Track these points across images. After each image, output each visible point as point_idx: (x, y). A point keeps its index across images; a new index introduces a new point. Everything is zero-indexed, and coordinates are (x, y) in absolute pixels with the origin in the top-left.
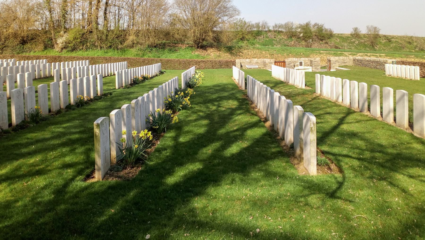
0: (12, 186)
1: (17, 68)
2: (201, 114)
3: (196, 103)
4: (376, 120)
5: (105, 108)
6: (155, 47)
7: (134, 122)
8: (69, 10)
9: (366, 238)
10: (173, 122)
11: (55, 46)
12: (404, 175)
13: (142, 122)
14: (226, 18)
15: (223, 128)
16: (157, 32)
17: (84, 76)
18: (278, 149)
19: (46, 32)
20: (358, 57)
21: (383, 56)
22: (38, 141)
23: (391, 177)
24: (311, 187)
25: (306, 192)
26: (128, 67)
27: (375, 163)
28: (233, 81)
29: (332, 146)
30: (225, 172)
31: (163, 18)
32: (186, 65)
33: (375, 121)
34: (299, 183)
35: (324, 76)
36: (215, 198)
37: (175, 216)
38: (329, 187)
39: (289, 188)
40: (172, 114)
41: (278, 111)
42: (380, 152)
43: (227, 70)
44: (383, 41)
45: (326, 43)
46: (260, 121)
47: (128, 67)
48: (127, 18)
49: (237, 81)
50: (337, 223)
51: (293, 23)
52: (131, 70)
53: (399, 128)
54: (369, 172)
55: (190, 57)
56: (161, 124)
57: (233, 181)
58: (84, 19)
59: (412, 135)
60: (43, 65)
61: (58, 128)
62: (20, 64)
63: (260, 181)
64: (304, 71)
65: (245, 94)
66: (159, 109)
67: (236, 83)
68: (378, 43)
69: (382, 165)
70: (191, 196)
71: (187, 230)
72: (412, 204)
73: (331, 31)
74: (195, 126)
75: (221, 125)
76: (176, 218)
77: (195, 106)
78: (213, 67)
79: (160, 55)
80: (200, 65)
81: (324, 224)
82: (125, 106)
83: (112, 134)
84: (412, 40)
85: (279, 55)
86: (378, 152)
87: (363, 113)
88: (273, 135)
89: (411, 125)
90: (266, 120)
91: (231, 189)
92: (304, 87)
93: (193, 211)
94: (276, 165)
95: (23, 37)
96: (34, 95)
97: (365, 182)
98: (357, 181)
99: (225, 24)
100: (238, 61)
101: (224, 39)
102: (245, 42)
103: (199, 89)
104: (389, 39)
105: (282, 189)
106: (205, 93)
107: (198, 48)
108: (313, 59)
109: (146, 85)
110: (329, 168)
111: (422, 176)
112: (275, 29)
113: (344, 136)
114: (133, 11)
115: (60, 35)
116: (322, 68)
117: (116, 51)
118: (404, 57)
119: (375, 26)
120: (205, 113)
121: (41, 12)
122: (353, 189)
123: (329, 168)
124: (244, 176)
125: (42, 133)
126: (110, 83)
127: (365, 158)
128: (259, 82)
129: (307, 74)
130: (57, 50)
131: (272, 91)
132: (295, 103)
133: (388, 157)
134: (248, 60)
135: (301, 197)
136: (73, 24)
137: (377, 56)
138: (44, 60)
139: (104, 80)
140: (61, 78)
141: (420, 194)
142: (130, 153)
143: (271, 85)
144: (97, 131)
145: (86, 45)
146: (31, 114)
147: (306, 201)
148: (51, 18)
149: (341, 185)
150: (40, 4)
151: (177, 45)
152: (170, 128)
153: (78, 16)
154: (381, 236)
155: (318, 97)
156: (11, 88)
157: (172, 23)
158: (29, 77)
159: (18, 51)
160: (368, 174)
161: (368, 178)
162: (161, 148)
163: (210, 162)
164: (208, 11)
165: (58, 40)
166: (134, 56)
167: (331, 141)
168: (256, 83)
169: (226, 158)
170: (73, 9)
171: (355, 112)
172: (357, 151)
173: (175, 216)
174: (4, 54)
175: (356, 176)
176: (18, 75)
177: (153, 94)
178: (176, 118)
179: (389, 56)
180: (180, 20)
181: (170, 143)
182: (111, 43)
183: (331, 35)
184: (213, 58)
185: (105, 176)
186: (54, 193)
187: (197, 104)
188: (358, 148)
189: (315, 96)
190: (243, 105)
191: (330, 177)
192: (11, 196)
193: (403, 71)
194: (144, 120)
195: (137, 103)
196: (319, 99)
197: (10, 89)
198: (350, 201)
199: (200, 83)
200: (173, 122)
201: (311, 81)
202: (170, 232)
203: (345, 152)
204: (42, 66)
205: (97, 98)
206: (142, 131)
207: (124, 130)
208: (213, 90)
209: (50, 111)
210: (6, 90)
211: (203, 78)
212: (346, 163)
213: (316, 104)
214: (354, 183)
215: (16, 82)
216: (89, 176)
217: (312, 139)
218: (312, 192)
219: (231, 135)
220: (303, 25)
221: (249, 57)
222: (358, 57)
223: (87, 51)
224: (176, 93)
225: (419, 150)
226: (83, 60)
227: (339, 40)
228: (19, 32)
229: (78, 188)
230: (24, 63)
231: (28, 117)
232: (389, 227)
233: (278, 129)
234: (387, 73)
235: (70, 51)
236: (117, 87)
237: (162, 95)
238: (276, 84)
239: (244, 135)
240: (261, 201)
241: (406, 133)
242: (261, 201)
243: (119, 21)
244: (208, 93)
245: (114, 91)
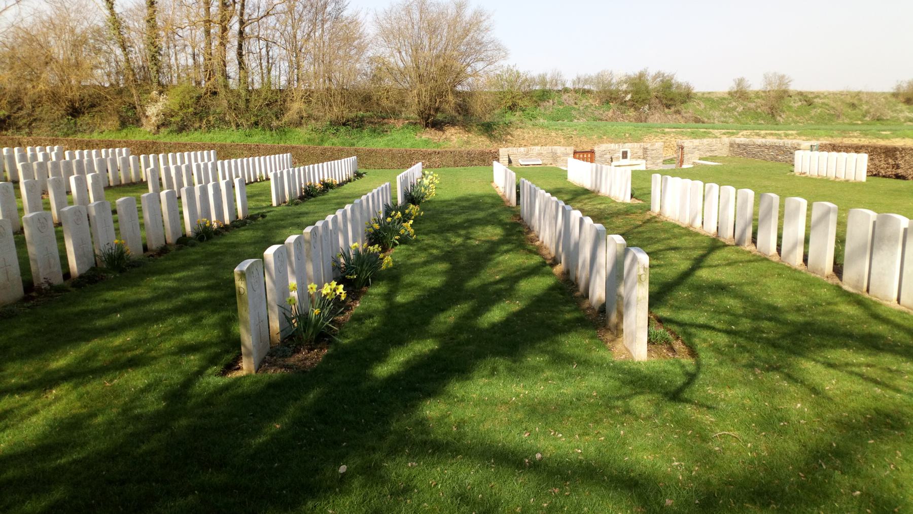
0: (82, 389)
1: (68, 165)
2: (435, 251)
4: (767, 260)
5: (254, 243)
6: (344, 124)
7: (310, 268)
8: (164, 44)
9: (736, 472)
10: (384, 267)
11: (144, 120)
12: (817, 361)
13: (326, 267)
14: (480, 66)
16: (348, 95)
17: (208, 182)
19: (120, 92)
20: (741, 138)
21: (792, 135)
22: (126, 306)
23: (789, 366)
24: (637, 382)
25: (627, 390)
26: (294, 165)
27: (760, 340)
29: (679, 308)
30: (480, 356)
31: (358, 66)
32: (405, 160)
33: (766, 262)
34: (613, 375)
35: (669, 177)
36: (462, 400)
37: (391, 433)
38: (669, 381)
40: (380, 252)
41: (577, 245)
42: (770, 319)
44: (796, 105)
45: (678, 112)
46: (544, 264)
47: (294, 165)
48: (285, 65)
50: (683, 446)
52: (299, 170)
53: (813, 275)
54: (747, 355)
55: (413, 144)
56: (361, 271)
57: (493, 372)
58: (196, 65)
60: (123, 159)
61: (164, 280)
62: (72, 156)
63: (543, 371)
65: (516, 213)
66: (356, 244)
67: (500, 194)
68: (785, 109)
69: (773, 344)
70: (419, 399)
71: (412, 456)
72: (829, 415)
74: (424, 274)
75: (471, 272)
76: (392, 437)
77: (424, 237)
78: (456, 164)
79: (355, 141)
80: (431, 159)
81: (657, 447)
82: (291, 239)
83: (271, 290)
84: (860, 100)
85: (583, 139)
87: (742, 247)
88: (569, 289)
89: (838, 269)
90: (555, 262)
91: (490, 384)
92: (628, 200)
93: (422, 423)
95: (72, 102)
96: (111, 217)
97: (739, 374)
98: (723, 371)
99: (480, 76)
100: (503, 152)
101: (477, 107)
102: (517, 114)
103: (430, 206)
104: (808, 100)
105: (584, 384)
106: (442, 212)
107: (427, 126)
108: (648, 146)
109: (329, 199)
110: (672, 349)
111: (853, 365)
112: (577, 87)
113: (702, 291)
114: (296, 51)
115: (152, 99)
117: (268, 133)
118: (836, 136)
120: (442, 251)
121: (105, 48)
122: (715, 385)
123: (672, 349)
124: (515, 362)
125: (134, 289)
126: (260, 195)
127: (740, 331)
128: (543, 191)
129: (635, 175)
130: (148, 130)
131: (568, 207)
132: (611, 230)
133: (786, 330)
134: (522, 149)
135: (618, 398)
136: (176, 75)
137: (779, 136)
138: (124, 150)
139: (248, 189)
140: (161, 185)
141: (846, 397)
142: (306, 323)
143: (566, 197)
144: (240, 284)
145: (208, 120)
146: (109, 255)
147: (627, 405)
148: (128, 61)
149: (691, 378)
150: (98, 32)
151: (386, 121)
152: (377, 277)
153: (185, 59)
154: (766, 470)
155: (655, 217)
156: (60, 205)
157: (375, 76)
158: (94, 184)
159: (65, 130)
160: (745, 358)
161: (744, 366)
162: (363, 315)
163: (452, 339)
164: (445, 50)
165: (148, 109)
166: (305, 142)
167: (676, 300)
169: (481, 331)
170: (171, 45)
171: (727, 246)
172: (727, 317)
173: (391, 433)
174: (34, 136)
176: (72, 179)
177: (344, 215)
178: (388, 260)
179: (804, 135)
180: (390, 71)
181: (379, 306)
182: (257, 116)
183: (687, 96)
184: (457, 145)
185: (262, 365)
186: (165, 398)
187: (426, 234)
188: (727, 312)
189: (648, 217)
190: (513, 235)
191: (672, 365)
192: (81, 407)
194: (329, 264)
195: (314, 232)
196: (656, 222)
197: (57, 207)
198: (709, 408)
199: (432, 193)
200: (384, 267)
201: (642, 189)
202: (382, 461)
203: (702, 320)
204: (120, 159)
205: (237, 224)
206: (326, 284)
207: (293, 282)
208: (457, 207)
209: (145, 248)
210: (50, 209)
211: (435, 183)
212: (703, 340)
213: (650, 231)
214: (718, 374)
215: (69, 192)
216: (233, 365)
217: (640, 296)
218: (638, 390)
219: (491, 289)
220: (633, 76)
222: (741, 139)
223: (209, 131)
224: (387, 213)
225: (849, 317)
226: (203, 149)
227: (703, 106)
228: (63, 91)
229: (211, 389)
230: (81, 155)
231: (102, 261)
232: (781, 454)
233: (576, 278)
234: (798, 169)
235: (176, 131)
236: (274, 204)
237: (361, 217)
238: (576, 196)
240: (545, 405)
241: (827, 284)
242: (545, 405)
243: (269, 72)
244: (448, 212)
245: (269, 209)
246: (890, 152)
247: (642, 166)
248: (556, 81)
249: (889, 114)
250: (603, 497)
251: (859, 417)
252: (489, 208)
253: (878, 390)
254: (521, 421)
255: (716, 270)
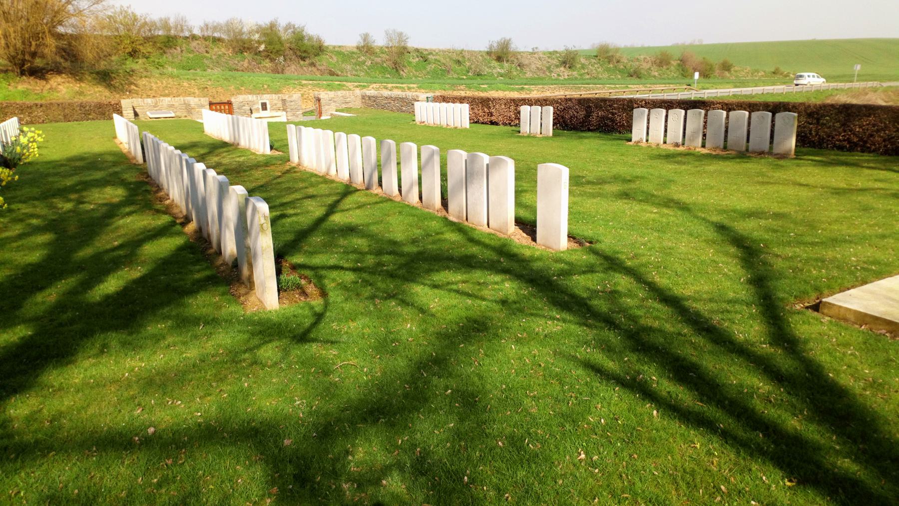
2: (34, 221)
3: (23, 198)
4: (391, 200)
12: (425, 285)
15: (88, 245)
18: (208, 273)
25: (256, 341)
28: (117, 147)
30: (87, 334)
33: (389, 203)
35: (302, 127)
36: (61, 389)
39: (224, 339)
41: (204, 200)
42: (390, 253)
43: (101, 124)
45: (313, 65)
46: (173, 224)
49: (126, 146)
50: (306, 384)
51: (243, 20)
54: (369, 288)
57: (104, 350)
59: (446, 219)
64: (265, 121)
65: (143, 171)
67: (125, 151)
69: (392, 275)
72: (431, 329)
73: (319, 40)
74: (18, 249)
77: (20, 206)
78: (67, 118)
80: (28, 114)
84: (463, 57)
85: (220, 90)
86: (388, 253)
87: (372, 191)
88: (202, 246)
90: (187, 220)
92: (268, 151)
94: (201, 303)
97: (361, 307)
98: (347, 306)
100: (126, 103)
101: (89, 54)
102: (140, 61)
103: (30, 169)
104: (424, 56)
105: (210, 343)
106: (48, 175)
107: (22, 73)
108: (286, 97)
110: (304, 293)
111: (453, 283)
112: (206, 34)
116: (304, 114)
119: (399, 30)
123: (304, 293)
124: (131, 334)
133: (402, 260)
134: (149, 101)
135: (245, 352)
137: (403, 89)
149: (319, 317)
155: (294, 168)
160: (367, 291)
168: (161, 148)
169: (92, 306)
172: (352, 256)
175: (346, 299)
183: (320, 49)
188: (355, 251)
189: (288, 168)
191: (297, 310)
193: (444, 114)
196: (295, 172)
198: (332, 343)
199: (34, 153)
203: (332, 262)
212: (332, 279)
213: (288, 181)
214: (343, 310)
217: (264, 245)
218: (267, 339)
219: (106, 258)
220: (264, 26)
221: (152, 93)
222: (370, 92)
225: (453, 243)
227: (335, 59)
233: (209, 236)
234: (418, 118)
238: (210, 150)
239: (136, 255)
242: (163, 374)
244: (56, 174)
246: (485, 102)
247: (282, 117)
248: (182, 26)
249: (486, 70)
250: (220, 456)
251: (454, 326)
252: (110, 167)
253: (469, 302)
254: (133, 398)
255: (347, 214)
